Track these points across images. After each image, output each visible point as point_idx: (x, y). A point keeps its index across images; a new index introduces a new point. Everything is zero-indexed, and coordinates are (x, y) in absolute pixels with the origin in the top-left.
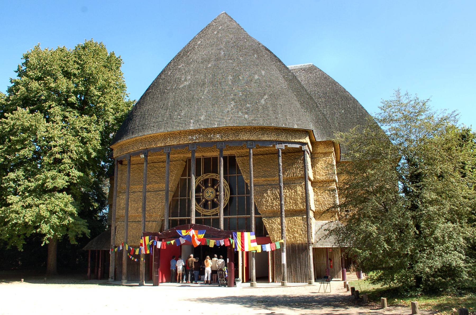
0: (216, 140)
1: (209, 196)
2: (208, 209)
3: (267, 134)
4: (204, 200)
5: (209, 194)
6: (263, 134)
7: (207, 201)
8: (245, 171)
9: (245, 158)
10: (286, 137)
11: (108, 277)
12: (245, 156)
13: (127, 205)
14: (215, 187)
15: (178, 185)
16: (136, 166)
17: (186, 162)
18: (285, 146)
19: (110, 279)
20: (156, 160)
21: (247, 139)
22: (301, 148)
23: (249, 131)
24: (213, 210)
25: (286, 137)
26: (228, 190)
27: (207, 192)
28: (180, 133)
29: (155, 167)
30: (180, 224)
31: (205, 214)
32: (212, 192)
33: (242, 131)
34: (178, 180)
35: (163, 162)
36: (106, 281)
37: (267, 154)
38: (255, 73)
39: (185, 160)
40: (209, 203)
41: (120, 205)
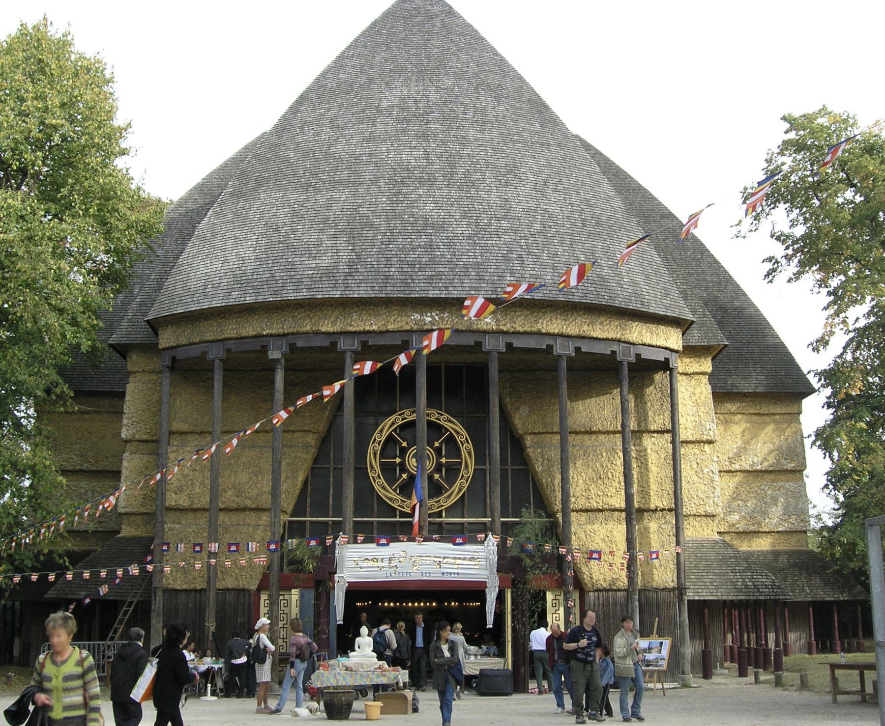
0: (485, 328)
4: (405, 476)
21: (556, 331)
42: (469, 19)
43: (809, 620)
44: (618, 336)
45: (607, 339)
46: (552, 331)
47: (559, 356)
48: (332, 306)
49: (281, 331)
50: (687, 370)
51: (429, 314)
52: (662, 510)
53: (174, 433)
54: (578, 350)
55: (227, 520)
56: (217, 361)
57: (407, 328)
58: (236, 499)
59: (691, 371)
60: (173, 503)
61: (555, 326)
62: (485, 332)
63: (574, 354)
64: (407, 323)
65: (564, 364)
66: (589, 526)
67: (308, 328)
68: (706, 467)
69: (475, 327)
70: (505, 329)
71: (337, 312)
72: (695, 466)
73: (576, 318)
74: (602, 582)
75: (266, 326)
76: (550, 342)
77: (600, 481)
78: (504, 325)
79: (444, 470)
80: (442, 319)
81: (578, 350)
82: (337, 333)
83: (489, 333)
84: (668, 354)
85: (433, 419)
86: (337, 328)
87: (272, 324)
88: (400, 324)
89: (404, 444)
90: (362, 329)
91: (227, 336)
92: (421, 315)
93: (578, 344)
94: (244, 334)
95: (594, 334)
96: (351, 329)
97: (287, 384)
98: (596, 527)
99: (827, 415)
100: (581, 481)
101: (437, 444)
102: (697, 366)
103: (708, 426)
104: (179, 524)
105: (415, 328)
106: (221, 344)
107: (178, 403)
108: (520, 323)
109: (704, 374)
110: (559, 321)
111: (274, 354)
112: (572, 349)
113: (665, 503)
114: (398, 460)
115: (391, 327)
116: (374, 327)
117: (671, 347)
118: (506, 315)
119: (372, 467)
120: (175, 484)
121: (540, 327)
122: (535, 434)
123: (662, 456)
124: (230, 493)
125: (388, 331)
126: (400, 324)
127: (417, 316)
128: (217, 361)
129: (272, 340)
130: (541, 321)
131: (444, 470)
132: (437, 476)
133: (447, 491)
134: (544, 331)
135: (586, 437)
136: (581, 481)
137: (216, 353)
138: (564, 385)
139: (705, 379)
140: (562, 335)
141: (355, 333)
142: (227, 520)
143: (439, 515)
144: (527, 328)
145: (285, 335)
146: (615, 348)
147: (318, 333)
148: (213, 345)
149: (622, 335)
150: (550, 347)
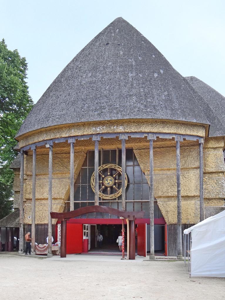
1: (109, 183)
2: (107, 194)
3: (168, 127)
4: (103, 187)
5: (109, 181)
6: (164, 127)
7: (106, 188)
8: (142, 162)
9: (142, 150)
10: (185, 130)
11: (17, 250)
12: (143, 149)
13: (34, 189)
14: (114, 176)
15: (79, 173)
16: (40, 156)
17: (87, 154)
18: (129, 137)
19: (20, 252)
20: (59, 152)
21: (148, 131)
22: (198, 141)
23: (150, 124)
24: (112, 195)
25: (185, 130)
26: (92, 184)
27: (107, 180)
28: (139, 132)
29: (59, 158)
30: (81, 207)
31: (104, 198)
32: (111, 180)
33: (144, 124)
34: (79, 169)
35: (65, 153)
36: (17, 252)
37: (163, 147)
38: (154, 72)
39: (86, 152)
40: (109, 189)
41: (27, 190)
42: (201, 80)
43: (210, 271)
44: (175, 132)
45: (170, 133)
46: (146, 131)
48: (65, 128)
49: (50, 138)
50: (213, 147)
52: (196, 196)
56: (34, 150)
58: (47, 196)
59: (215, 146)
61: (148, 129)
62: (120, 133)
67: (58, 136)
68: (220, 181)
70: (127, 131)
72: (215, 181)
73: (157, 126)
74: (172, 222)
75: (46, 137)
76: (146, 135)
80: (103, 129)
82: (67, 137)
83: (121, 133)
85: (113, 167)
86: (67, 135)
87: (47, 136)
89: (103, 176)
91: (35, 141)
94: (40, 140)
95: (164, 131)
96: (72, 135)
97: (53, 157)
102: (218, 145)
103: (221, 166)
106: (34, 144)
107: (29, 166)
109: (221, 147)
113: (198, 194)
114: (117, 181)
115: (85, 133)
117: (200, 135)
121: (141, 130)
123: (197, 177)
125: (84, 135)
128: (34, 150)
129: (48, 141)
133: (118, 191)
134: (143, 131)
139: (221, 150)
140: (150, 133)
141: (73, 136)
143: (115, 199)
144: (136, 130)
145: (52, 139)
146: (174, 136)
147: (62, 138)
148: (33, 145)
150: (146, 137)
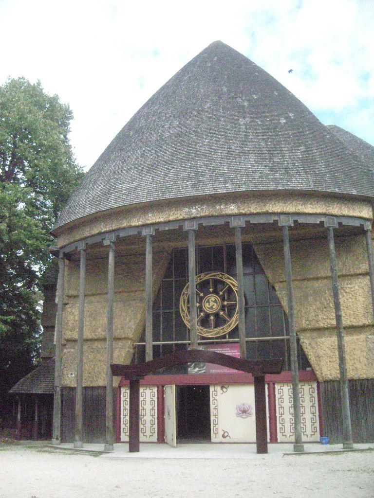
0: (230, 212)
4: (202, 314)
21: (279, 211)
46: (276, 211)
47: (283, 227)
51: (194, 208)
53: (87, 295)
54: (340, 224)
55: (99, 346)
56: (82, 251)
57: (181, 217)
58: (103, 333)
60: (70, 337)
61: (278, 207)
63: (338, 227)
64: (181, 215)
65: (331, 234)
66: (319, 339)
67: (125, 225)
69: (224, 213)
70: (244, 212)
71: (140, 213)
76: (276, 218)
77: (325, 310)
78: (243, 209)
79: (226, 309)
80: (202, 209)
81: (340, 224)
84: (362, 222)
85: (218, 278)
86: (140, 223)
88: (176, 216)
90: (154, 221)
92: (190, 209)
93: (296, 218)
95: (306, 211)
96: (149, 222)
98: (323, 339)
99: (19, 283)
100: (312, 310)
101: (221, 293)
104: (74, 349)
105: (186, 217)
108: (254, 208)
110: (281, 204)
111: (107, 243)
112: (336, 223)
113: (370, 321)
115: (171, 218)
116: (162, 220)
118: (244, 203)
119: (183, 310)
120: (71, 326)
121: (268, 209)
122: (281, 282)
124: (100, 330)
125: (170, 221)
126: (176, 216)
127: (187, 210)
130: (268, 205)
131: (226, 309)
132: (222, 313)
134: (270, 211)
135: (315, 282)
136: (312, 310)
137: (82, 246)
138: (332, 246)
142: (99, 346)
144: (259, 210)
145: (113, 231)
146: (323, 219)
147: (131, 227)
149: (327, 210)
